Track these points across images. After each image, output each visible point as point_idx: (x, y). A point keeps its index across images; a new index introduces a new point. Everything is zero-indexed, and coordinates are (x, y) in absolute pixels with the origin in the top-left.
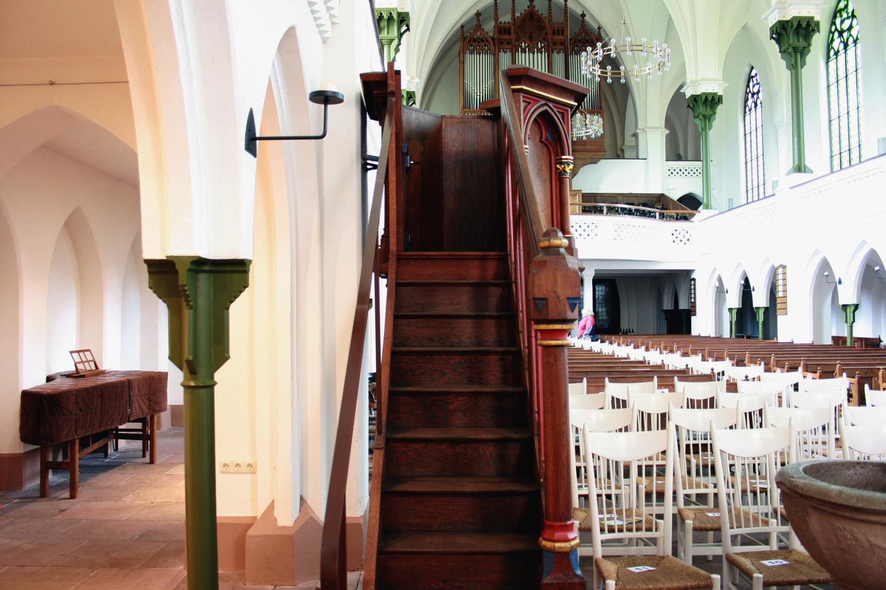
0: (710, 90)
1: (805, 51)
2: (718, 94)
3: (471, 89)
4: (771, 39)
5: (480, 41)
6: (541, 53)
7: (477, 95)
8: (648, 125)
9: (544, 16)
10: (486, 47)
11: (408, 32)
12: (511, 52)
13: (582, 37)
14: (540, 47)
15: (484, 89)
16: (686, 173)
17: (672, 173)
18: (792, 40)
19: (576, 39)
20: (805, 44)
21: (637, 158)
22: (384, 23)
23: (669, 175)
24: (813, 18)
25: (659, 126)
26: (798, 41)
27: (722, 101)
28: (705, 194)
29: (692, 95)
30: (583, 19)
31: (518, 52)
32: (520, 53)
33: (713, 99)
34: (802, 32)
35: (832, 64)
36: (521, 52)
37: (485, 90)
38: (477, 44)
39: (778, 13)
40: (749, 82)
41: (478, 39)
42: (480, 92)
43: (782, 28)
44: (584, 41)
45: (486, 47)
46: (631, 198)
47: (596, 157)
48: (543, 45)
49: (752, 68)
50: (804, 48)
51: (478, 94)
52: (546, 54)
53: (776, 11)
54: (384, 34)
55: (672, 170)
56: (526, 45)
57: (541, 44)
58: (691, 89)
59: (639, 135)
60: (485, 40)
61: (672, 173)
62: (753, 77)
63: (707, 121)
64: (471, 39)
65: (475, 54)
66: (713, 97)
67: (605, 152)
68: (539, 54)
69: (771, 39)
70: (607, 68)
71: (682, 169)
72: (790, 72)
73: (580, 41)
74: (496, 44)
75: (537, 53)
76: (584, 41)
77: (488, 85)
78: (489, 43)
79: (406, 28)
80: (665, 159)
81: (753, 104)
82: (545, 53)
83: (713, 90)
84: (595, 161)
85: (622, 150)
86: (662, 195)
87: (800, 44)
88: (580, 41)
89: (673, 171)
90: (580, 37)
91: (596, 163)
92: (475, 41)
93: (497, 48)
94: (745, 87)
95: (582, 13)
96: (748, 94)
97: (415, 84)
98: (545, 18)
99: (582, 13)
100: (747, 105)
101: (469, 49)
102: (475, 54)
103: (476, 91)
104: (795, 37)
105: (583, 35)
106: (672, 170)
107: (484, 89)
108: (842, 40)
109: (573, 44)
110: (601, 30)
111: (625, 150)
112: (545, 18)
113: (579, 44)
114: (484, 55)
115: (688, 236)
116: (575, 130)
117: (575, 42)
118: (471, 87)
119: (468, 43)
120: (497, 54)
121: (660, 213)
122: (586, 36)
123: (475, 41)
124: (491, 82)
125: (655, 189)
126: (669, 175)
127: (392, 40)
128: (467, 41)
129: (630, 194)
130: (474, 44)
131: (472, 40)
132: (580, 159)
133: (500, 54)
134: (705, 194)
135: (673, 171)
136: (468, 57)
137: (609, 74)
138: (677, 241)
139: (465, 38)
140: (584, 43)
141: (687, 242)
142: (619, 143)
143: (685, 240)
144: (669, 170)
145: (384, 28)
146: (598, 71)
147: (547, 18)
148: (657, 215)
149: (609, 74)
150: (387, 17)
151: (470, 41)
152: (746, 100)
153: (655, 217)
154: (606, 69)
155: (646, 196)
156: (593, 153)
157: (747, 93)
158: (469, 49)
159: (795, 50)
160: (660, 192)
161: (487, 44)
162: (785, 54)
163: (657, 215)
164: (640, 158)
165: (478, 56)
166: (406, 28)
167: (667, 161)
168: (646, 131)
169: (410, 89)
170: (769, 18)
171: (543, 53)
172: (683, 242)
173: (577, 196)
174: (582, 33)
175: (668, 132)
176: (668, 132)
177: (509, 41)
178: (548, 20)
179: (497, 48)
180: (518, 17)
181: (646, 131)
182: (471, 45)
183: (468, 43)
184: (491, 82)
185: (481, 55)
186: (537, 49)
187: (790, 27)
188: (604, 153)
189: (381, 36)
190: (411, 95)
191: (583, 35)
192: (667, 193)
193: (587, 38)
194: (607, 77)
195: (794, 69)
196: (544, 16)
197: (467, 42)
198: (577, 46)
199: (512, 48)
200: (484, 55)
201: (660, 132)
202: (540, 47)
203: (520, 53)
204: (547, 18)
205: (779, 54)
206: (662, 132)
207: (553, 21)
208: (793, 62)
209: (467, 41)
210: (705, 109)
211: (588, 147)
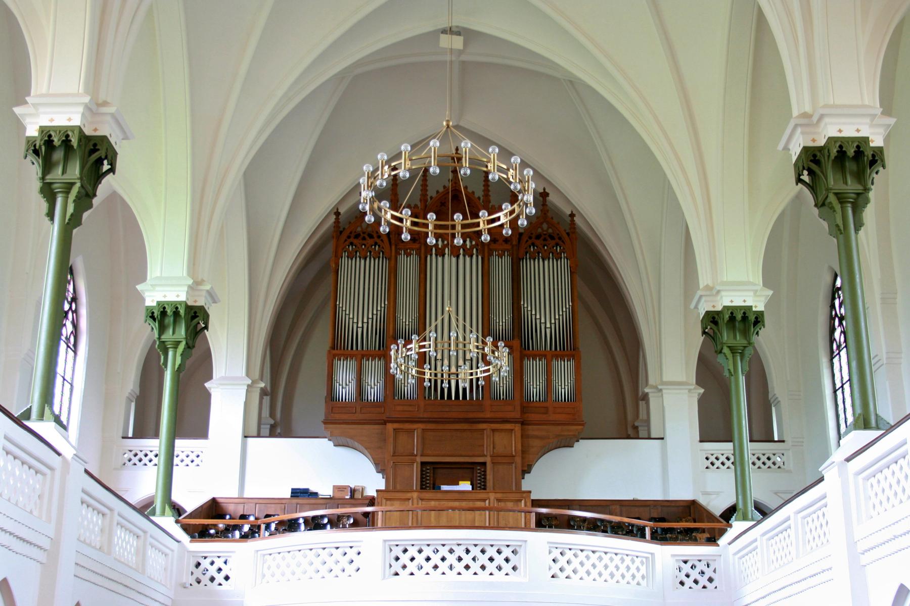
0: (738, 302)
1: (861, 200)
2: (754, 309)
3: (344, 313)
4: (797, 184)
5: (366, 237)
6: (471, 256)
7: (357, 327)
8: (665, 379)
9: (477, 195)
10: (377, 247)
11: (112, 174)
12: (419, 254)
13: (542, 229)
14: (468, 247)
15: (370, 316)
16: (718, 463)
17: (712, 464)
18: (832, 180)
19: (532, 234)
20: (858, 188)
21: (650, 438)
22: (58, 155)
23: (707, 468)
24: (866, 140)
25: (684, 379)
26: (846, 183)
27: (883, 160)
28: (740, 497)
29: (707, 312)
30: (545, 200)
31: (431, 255)
32: (434, 256)
33: (745, 318)
34: (850, 166)
35: (836, 360)
36: (436, 255)
37: (373, 318)
38: (361, 242)
39: (802, 133)
40: (833, 299)
41: (364, 233)
42: (363, 322)
43: (811, 161)
44: (547, 237)
45: (377, 247)
46: (637, 509)
47: (566, 433)
48: (474, 243)
49: (836, 276)
50: (858, 194)
51: (360, 325)
52: (480, 258)
53: (799, 130)
54: (57, 175)
55: (712, 459)
56: (446, 242)
57: (471, 242)
58: (706, 301)
59: (650, 395)
60: (375, 235)
61: (712, 464)
62: (839, 289)
63: (739, 358)
64: (351, 233)
65: (358, 259)
66: (744, 313)
67: (583, 425)
68: (468, 259)
69: (797, 184)
70: (429, 216)
71: (720, 456)
72: (835, 240)
73: (538, 237)
74: (393, 242)
75: (464, 256)
76: (547, 237)
77: (377, 310)
78: (382, 240)
79: (109, 167)
80: (698, 439)
81: (843, 336)
82: (477, 256)
83: (745, 301)
84: (568, 443)
85: (636, 428)
86: (694, 502)
87: (848, 188)
88: (538, 237)
89: (715, 461)
90: (540, 230)
91: (571, 446)
92: (357, 236)
93: (393, 247)
94: (829, 308)
95: (542, 191)
96: (834, 319)
97: (204, 293)
98: (479, 198)
99: (542, 191)
100: (835, 339)
101: (348, 250)
102: (358, 259)
103: (355, 320)
104: (839, 176)
105: (545, 226)
106: (712, 459)
107: (370, 316)
108: (843, 330)
109: (527, 241)
110: (575, 218)
111: (640, 428)
112: (479, 198)
113: (538, 242)
114: (372, 259)
115: (709, 573)
116: (493, 379)
117: (530, 238)
118: (347, 313)
119: (346, 240)
120: (393, 257)
121: (652, 529)
122: (549, 228)
123: (357, 236)
124: (383, 305)
125: (681, 492)
126: (707, 468)
127: (73, 184)
128: (344, 236)
129: (633, 500)
130: (356, 241)
131: (352, 236)
132: (537, 437)
133: (399, 258)
134: (740, 497)
135: (715, 461)
136: (345, 261)
137: (431, 227)
138: (689, 582)
139: (341, 232)
140: (545, 240)
141: (707, 584)
142: (630, 417)
143: (703, 581)
144: (707, 459)
145: (56, 164)
146: (406, 220)
147: (482, 198)
148: (648, 532)
149: (431, 227)
150: (60, 142)
151: (349, 237)
152: (832, 330)
153: (643, 536)
154: (427, 219)
155: (666, 504)
156: (560, 428)
157: (832, 319)
158: (348, 250)
159: (841, 198)
160: (693, 499)
161: (378, 241)
162: (825, 209)
163: (648, 532)
164: (640, 436)
165: (363, 261)
166: (109, 167)
167: (701, 441)
168: (661, 390)
169: (195, 301)
170: (791, 147)
171: (474, 256)
172: (701, 585)
173: (523, 501)
174: (542, 223)
175: (702, 391)
176: (702, 391)
177: (416, 236)
178: (483, 202)
179: (393, 247)
180: (431, 198)
181: (661, 390)
182: (352, 244)
183: (346, 240)
184: (383, 305)
185: (368, 259)
186: (464, 250)
187: (826, 158)
188: (580, 427)
189: (49, 178)
190: (195, 313)
191: (545, 226)
192: (702, 501)
193: (550, 231)
194: (427, 233)
195: (841, 233)
196: (477, 195)
197: (345, 238)
198: (533, 245)
199: (420, 249)
200: (372, 259)
201: (687, 391)
202: (468, 247)
203: (434, 256)
204: (482, 198)
205: (816, 211)
206: (690, 390)
207: (491, 204)
208: (839, 221)
209: (344, 236)
210: (732, 336)
211: (552, 417)
